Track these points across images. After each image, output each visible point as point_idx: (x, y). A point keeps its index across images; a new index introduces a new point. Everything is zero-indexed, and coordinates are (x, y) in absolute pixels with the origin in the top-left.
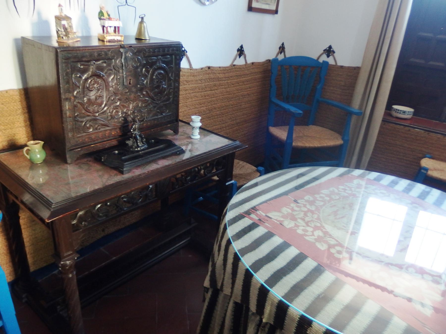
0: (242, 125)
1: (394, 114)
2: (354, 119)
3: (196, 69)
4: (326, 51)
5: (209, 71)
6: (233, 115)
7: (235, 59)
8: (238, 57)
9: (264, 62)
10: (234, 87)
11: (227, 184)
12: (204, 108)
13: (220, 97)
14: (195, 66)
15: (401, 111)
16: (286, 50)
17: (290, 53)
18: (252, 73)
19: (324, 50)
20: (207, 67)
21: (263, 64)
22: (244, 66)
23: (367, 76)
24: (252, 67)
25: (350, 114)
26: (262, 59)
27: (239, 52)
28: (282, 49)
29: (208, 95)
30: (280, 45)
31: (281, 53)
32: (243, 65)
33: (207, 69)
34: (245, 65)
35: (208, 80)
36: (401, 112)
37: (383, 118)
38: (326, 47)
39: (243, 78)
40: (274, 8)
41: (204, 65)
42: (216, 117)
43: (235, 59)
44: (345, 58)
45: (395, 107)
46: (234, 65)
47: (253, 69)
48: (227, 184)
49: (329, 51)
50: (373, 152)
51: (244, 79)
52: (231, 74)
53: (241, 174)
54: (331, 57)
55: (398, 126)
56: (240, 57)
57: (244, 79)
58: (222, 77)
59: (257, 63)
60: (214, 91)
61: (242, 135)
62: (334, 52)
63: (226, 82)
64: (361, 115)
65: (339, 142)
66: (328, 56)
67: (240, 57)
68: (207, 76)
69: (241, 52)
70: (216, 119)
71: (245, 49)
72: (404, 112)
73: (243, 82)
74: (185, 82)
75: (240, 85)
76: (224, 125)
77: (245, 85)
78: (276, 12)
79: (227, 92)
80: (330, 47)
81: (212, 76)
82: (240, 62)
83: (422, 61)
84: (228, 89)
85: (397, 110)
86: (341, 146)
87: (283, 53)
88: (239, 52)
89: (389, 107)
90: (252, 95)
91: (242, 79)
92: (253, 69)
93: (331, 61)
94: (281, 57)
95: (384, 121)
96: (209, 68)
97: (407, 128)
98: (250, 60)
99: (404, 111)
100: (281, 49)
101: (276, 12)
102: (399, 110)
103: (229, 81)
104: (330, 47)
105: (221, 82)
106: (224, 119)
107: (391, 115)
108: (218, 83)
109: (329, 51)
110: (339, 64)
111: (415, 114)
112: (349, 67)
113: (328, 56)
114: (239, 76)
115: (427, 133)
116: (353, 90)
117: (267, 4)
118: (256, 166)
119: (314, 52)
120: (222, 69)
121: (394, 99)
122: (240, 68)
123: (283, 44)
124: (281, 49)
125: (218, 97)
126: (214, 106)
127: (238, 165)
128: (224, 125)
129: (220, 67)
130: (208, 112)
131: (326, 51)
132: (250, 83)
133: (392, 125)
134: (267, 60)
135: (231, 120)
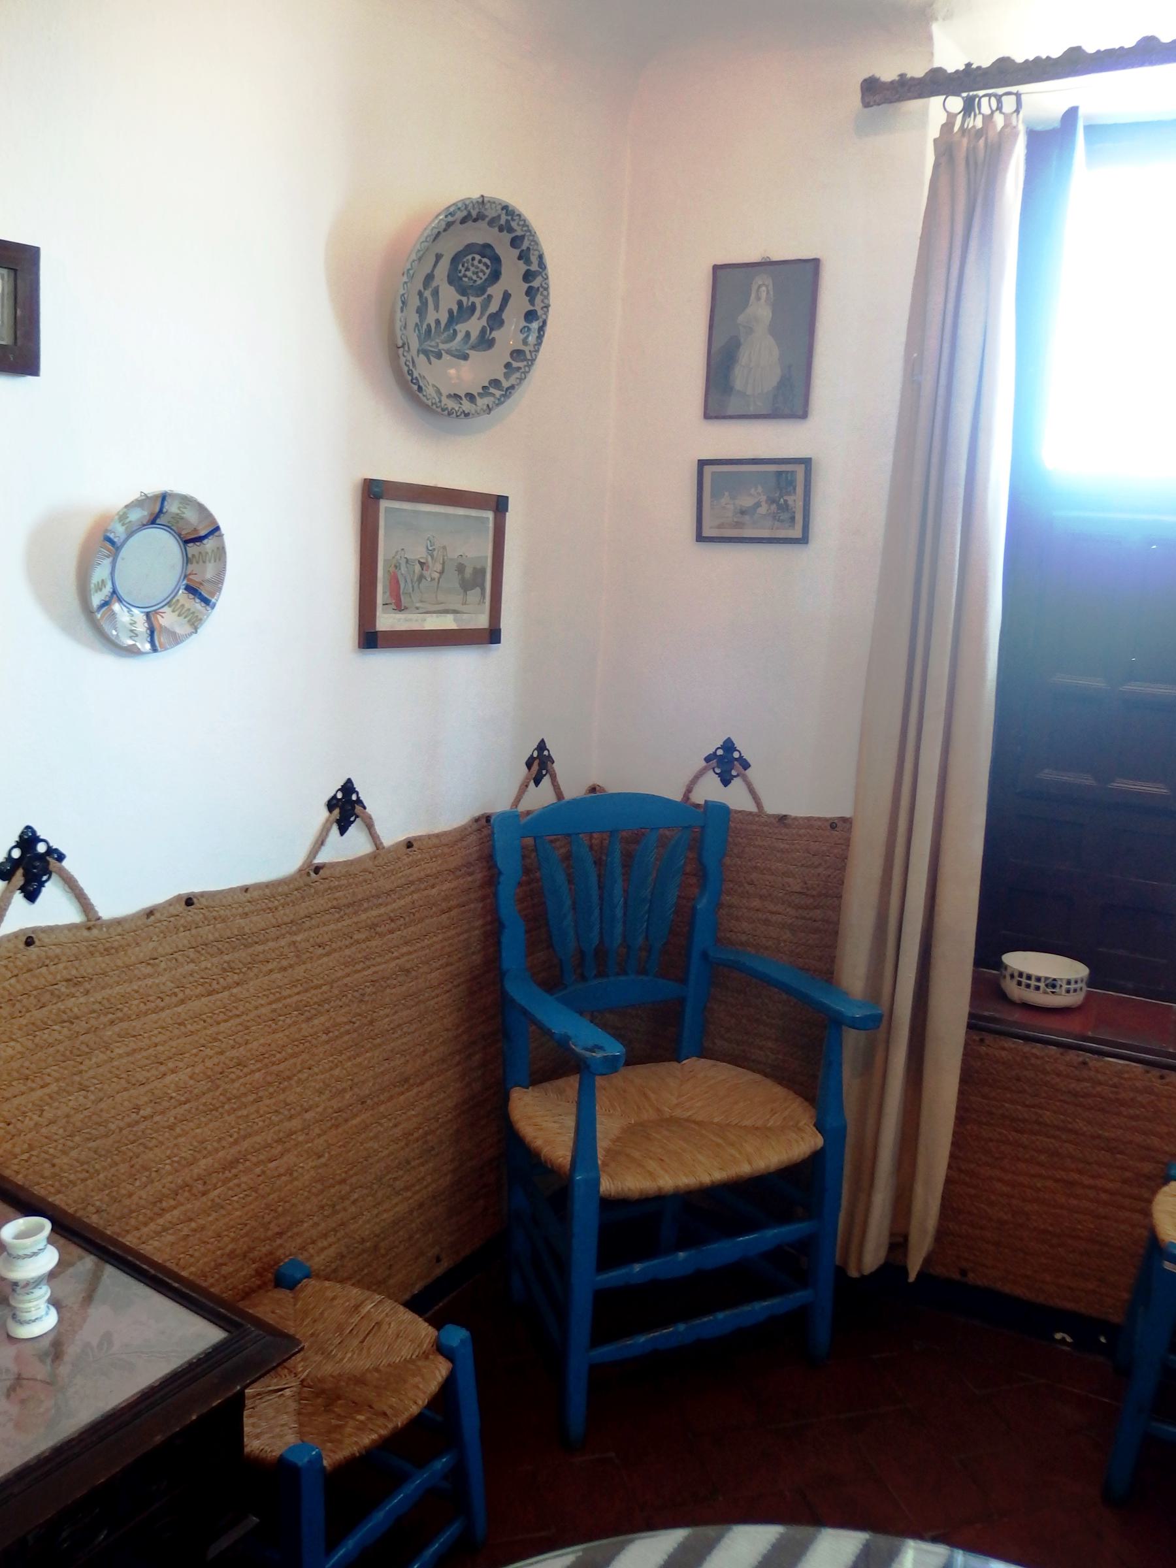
0: (391, 1098)
1: (1014, 991)
2: (852, 1039)
3: (118, 922)
4: (714, 762)
5: (193, 914)
6: (336, 1072)
7: (320, 842)
8: (335, 829)
9: (463, 829)
10: (328, 954)
11: (214, 1551)
12: (183, 1076)
13: (263, 1010)
14: (109, 908)
15: (1038, 979)
16: (559, 767)
17: (574, 776)
18: (412, 883)
19: (708, 759)
20: (179, 897)
21: (460, 835)
22: (369, 864)
23: (874, 889)
24: (407, 860)
25: (836, 1022)
26: (451, 814)
27: (337, 811)
28: (540, 764)
29: (197, 1017)
30: (529, 749)
31: (537, 782)
32: (359, 860)
33: (181, 907)
34: (374, 857)
35: (191, 953)
36: (1042, 985)
37: (971, 1016)
38: (713, 744)
39: (365, 910)
40: (481, 621)
41: (159, 893)
42: (252, 1097)
43: (320, 842)
44: (796, 781)
45: (1016, 960)
46: (317, 869)
47: (411, 865)
48: (214, 1551)
49: (727, 762)
50: (952, 1156)
51: (374, 913)
52: (303, 908)
53: (359, 1380)
54: (737, 783)
55: (1037, 1050)
56: (343, 831)
57: (374, 913)
58: (263, 925)
59: (429, 837)
60: (226, 993)
61: (396, 1141)
62: (746, 765)
63: (283, 942)
64: (876, 1023)
65: (803, 1143)
66: (726, 782)
67: (343, 831)
68: (183, 939)
69: (346, 807)
70: (252, 1109)
71: (364, 791)
72: (1053, 984)
73: (373, 926)
74: (63, 988)
75: (358, 942)
76: (296, 1124)
77: (381, 935)
78: (492, 635)
79: (294, 983)
80: (729, 746)
81: (208, 933)
82: (350, 846)
83: (1088, 780)
84: (299, 972)
85: (1023, 978)
86: (817, 1157)
87: (546, 781)
88: (337, 811)
89: (988, 955)
90: (425, 969)
91: (363, 916)
92: (411, 865)
93: (735, 797)
94: (540, 797)
95: (976, 1024)
96: (189, 901)
97: (1072, 1056)
98: (392, 833)
99: (1047, 972)
100: (535, 767)
101: (492, 635)
102: (1029, 977)
103: (298, 938)
104: (729, 746)
105: (260, 948)
106: (292, 1098)
107: (1002, 996)
108: (243, 954)
109: (727, 762)
110: (773, 807)
111: (1092, 982)
112: (809, 819)
113: (726, 782)
114: (349, 905)
115: (1156, 1072)
116: (837, 909)
117: (446, 612)
118: (437, 1323)
119: (665, 770)
120: (256, 894)
121: (1001, 927)
122: (351, 870)
123: (542, 746)
124: (535, 767)
125: (252, 1015)
126: (234, 1053)
127: (355, 1319)
128: (296, 1124)
129: (246, 889)
130: (204, 1085)
131: (714, 762)
132: (406, 926)
133: (1009, 1043)
134: (477, 820)
135: (327, 1094)
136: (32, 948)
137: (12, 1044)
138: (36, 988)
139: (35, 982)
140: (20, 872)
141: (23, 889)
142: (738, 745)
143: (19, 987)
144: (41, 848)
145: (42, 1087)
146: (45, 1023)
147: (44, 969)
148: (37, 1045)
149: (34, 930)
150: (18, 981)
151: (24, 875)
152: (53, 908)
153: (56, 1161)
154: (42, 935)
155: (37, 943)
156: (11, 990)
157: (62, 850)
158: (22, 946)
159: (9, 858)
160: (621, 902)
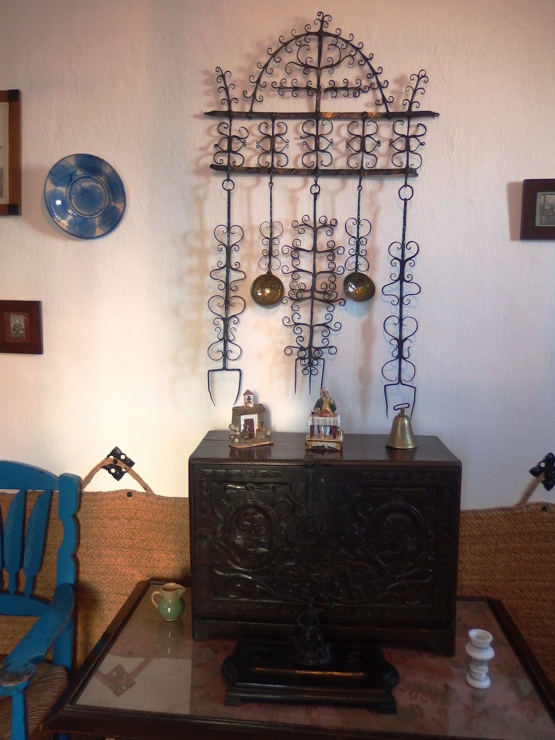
104: (116, 453)
129: (503, 509)
136: (545, 512)
137: (529, 555)
138: (544, 532)
139: (544, 529)
140: (543, 474)
141: (544, 482)
142: (534, 465)
143: (536, 528)
144: (543, 465)
145: (542, 581)
146: (547, 551)
147: (550, 524)
148: (541, 560)
149: (548, 504)
150: (536, 526)
151: (545, 476)
152: (127, 482)
153: (545, 621)
154: (552, 508)
155: (548, 510)
156: (531, 529)
157: (133, 460)
158: (540, 509)
159: (539, 466)
160: (113, 635)
